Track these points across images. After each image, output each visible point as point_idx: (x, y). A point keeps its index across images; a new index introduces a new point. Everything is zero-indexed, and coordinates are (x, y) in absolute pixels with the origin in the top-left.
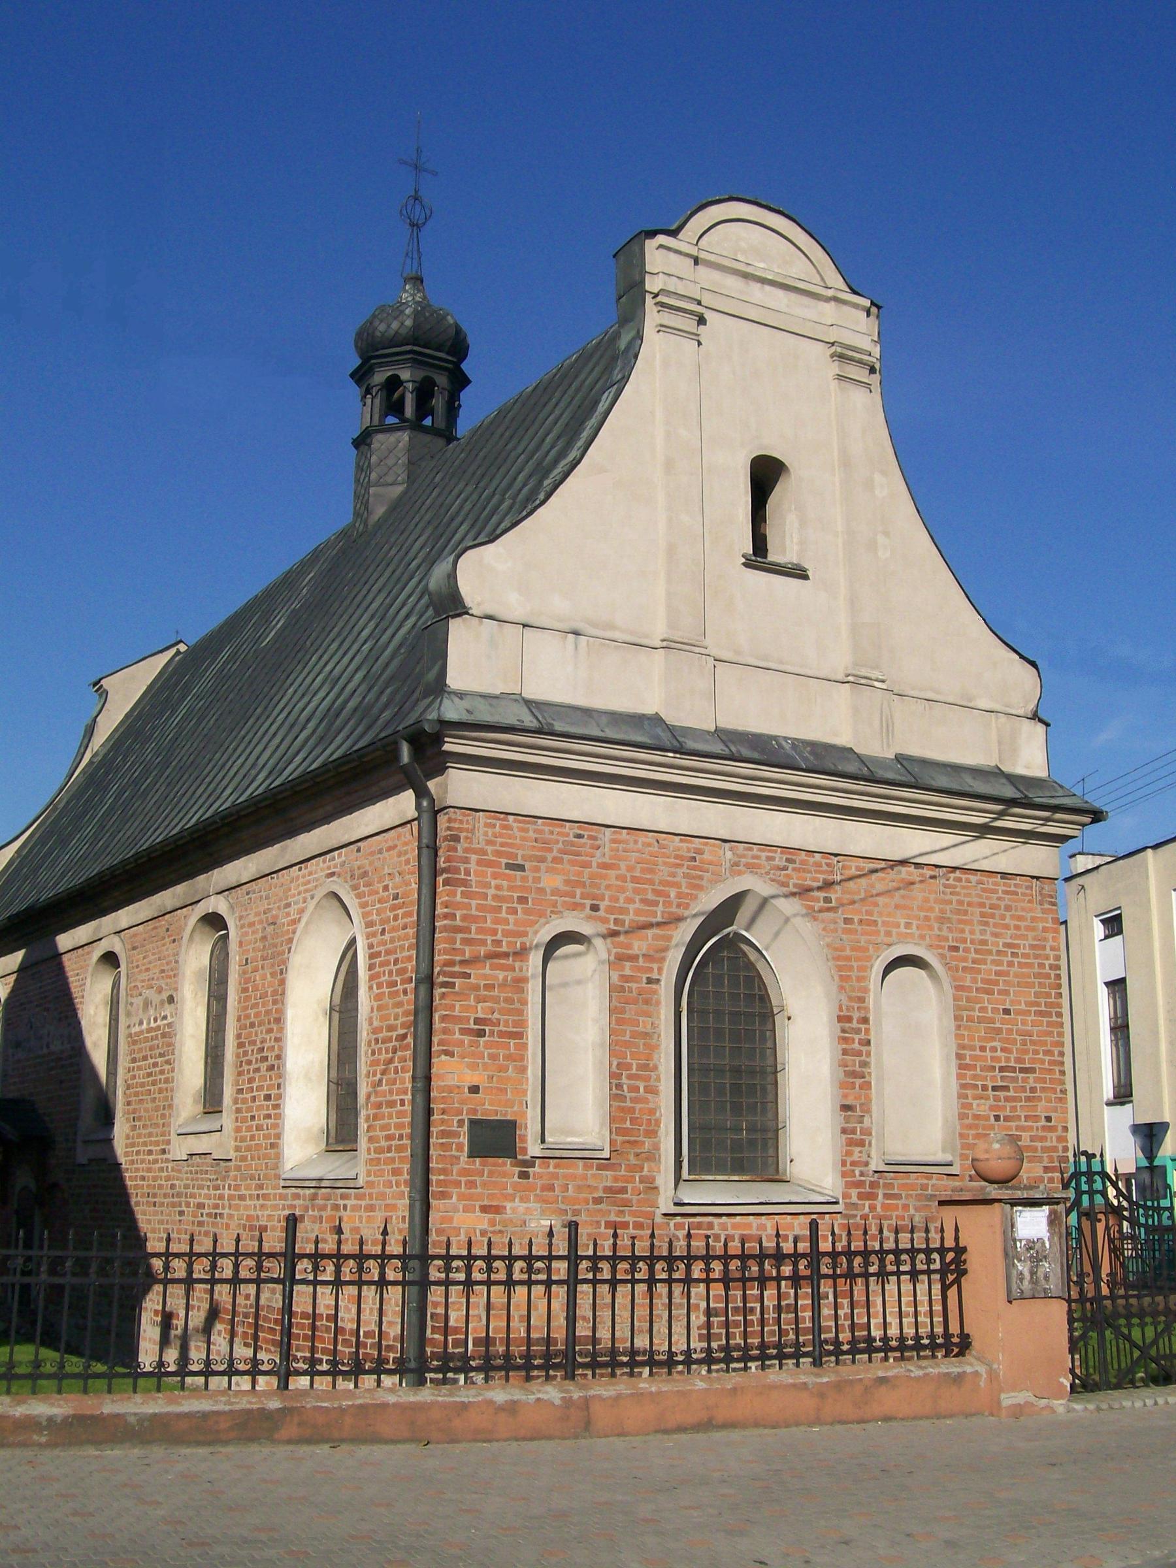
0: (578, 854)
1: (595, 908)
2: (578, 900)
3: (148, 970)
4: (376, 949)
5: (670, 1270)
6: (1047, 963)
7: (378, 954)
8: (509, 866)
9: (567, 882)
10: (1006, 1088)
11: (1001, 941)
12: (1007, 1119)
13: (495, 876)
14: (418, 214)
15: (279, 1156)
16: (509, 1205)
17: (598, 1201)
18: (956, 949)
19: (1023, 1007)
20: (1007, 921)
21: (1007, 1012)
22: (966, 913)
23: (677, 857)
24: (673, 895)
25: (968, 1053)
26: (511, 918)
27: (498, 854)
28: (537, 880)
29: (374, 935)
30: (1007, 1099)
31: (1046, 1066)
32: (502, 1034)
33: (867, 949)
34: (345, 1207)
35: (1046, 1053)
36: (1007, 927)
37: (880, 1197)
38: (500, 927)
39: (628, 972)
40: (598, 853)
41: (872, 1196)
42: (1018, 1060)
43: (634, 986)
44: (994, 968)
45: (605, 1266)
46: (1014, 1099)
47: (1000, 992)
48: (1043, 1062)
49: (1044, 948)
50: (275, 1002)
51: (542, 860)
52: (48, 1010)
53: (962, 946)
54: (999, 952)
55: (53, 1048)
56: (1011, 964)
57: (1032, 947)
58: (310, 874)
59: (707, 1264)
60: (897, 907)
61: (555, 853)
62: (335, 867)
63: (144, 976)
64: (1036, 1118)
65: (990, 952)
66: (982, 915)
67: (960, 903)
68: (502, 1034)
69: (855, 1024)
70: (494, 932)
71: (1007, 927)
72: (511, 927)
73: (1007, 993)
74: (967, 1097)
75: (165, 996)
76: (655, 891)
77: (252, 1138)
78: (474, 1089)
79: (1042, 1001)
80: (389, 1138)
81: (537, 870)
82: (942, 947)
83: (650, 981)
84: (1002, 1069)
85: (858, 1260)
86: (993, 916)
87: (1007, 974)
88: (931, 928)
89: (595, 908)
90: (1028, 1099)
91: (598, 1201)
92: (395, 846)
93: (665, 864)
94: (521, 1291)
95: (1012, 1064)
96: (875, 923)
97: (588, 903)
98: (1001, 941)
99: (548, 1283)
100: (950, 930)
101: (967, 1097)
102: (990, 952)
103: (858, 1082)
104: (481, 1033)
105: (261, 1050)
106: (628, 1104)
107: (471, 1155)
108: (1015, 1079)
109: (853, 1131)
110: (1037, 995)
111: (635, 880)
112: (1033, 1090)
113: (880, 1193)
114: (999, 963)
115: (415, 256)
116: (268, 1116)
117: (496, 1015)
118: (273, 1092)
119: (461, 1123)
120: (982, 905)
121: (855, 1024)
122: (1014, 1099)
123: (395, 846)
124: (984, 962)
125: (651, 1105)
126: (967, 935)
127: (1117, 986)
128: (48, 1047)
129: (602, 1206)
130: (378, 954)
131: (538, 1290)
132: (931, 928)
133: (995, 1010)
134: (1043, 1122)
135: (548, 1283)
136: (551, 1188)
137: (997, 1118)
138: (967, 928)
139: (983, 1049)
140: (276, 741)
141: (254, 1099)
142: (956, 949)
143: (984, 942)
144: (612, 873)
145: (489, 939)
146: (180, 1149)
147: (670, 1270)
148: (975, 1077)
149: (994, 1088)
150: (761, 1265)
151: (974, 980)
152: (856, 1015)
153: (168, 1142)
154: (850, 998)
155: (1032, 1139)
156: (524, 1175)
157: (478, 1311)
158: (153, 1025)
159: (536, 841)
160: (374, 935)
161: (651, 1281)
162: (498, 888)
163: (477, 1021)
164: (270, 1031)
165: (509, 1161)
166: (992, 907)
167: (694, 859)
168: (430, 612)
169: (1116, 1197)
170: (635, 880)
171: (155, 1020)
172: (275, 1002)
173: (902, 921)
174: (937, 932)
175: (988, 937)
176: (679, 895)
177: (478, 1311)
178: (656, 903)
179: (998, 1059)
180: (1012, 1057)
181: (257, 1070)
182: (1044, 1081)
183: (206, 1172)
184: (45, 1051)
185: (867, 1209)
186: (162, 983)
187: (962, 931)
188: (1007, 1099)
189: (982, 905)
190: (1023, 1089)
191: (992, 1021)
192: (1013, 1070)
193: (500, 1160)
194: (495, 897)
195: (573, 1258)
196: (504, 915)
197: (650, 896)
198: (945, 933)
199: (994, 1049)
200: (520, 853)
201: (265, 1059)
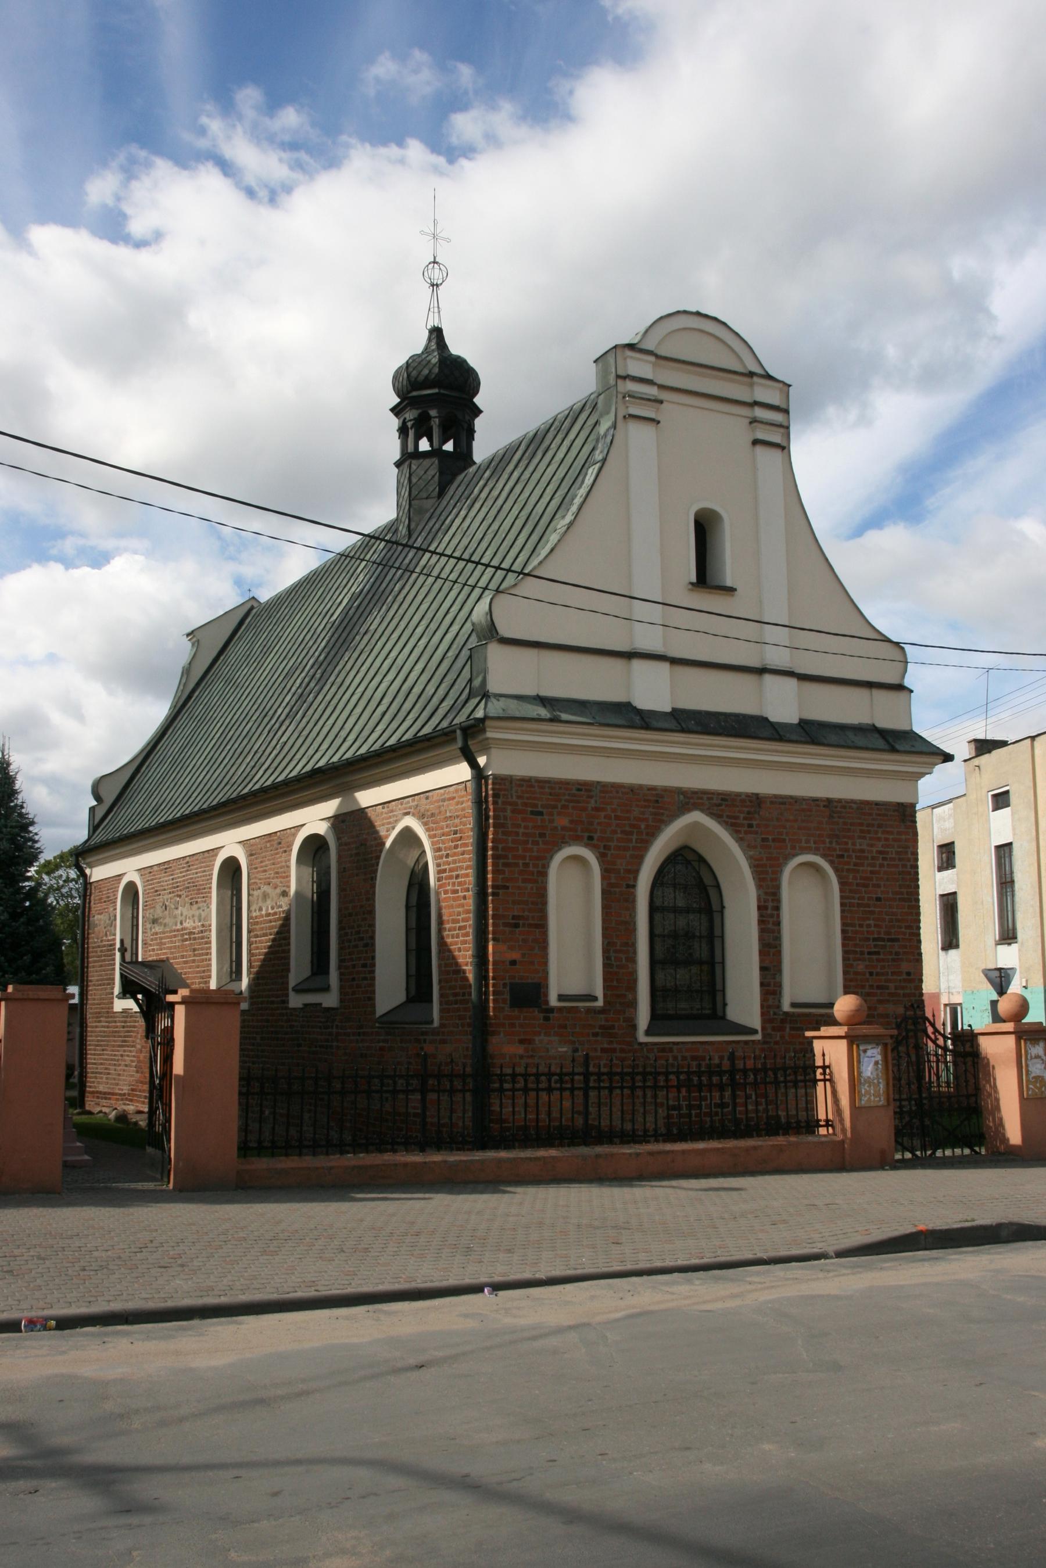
0: (578, 802)
1: (591, 838)
2: (579, 833)
3: (265, 871)
4: (443, 867)
5: (644, 1081)
6: (909, 864)
7: (444, 871)
8: (532, 813)
9: (571, 822)
10: (878, 953)
11: (874, 849)
12: (878, 974)
13: (524, 820)
14: (437, 275)
15: (373, 1006)
16: (537, 1038)
17: (595, 1035)
18: (842, 856)
19: (890, 895)
20: (879, 835)
21: (878, 899)
22: (849, 830)
23: (645, 801)
24: (643, 827)
25: (850, 929)
26: (535, 848)
27: (525, 805)
28: (551, 821)
29: (441, 857)
30: (878, 960)
31: (907, 936)
32: (530, 925)
33: (778, 859)
34: (425, 1041)
35: (907, 927)
36: (879, 839)
37: (788, 1029)
38: (528, 854)
39: (613, 881)
40: (593, 801)
41: (781, 1029)
42: (888, 933)
43: (617, 890)
44: (869, 869)
45: (521, 1079)
46: (883, 960)
47: (874, 886)
48: (904, 934)
49: (907, 853)
50: (368, 899)
51: (555, 807)
52: (180, 896)
53: (846, 854)
54: (873, 858)
55: (185, 925)
56: (882, 866)
57: (897, 853)
58: (392, 811)
59: (667, 1077)
60: (799, 828)
61: (563, 802)
62: (410, 808)
63: (261, 875)
64: (900, 973)
65: (867, 858)
66: (862, 831)
67: (845, 823)
68: (530, 925)
69: (769, 911)
70: (524, 858)
71: (879, 839)
72: (535, 854)
73: (879, 886)
74: (849, 959)
75: (278, 891)
76: (631, 826)
77: (354, 993)
78: (513, 963)
79: (904, 890)
80: (455, 995)
81: (551, 814)
82: (832, 856)
83: (628, 886)
84: (875, 940)
85: (662, 1078)
86: (869, 832)
87: (878, 872)
88: (824, 842)
89: (591, 838)
90: (893, 960)
91: (595, 1035)
92: (454, 798)
93: (637, 806)
94: (557, 1093)
95: (882, 936)
96: (784, 841)
97: (586, 834)
98: (874, 849)
99: (572, 1090)
100: (838, 843)
101: (849, 959)
102: (867, 858)
103: (772, 950)
104: (516, 926)
105: (358, 932)
106: (615, 969)
107: (512, 1006)
108: (884, 947)
109: (769, 985)
110: (900, 886)
111: (617, 818)
112: (897, 954)
113: (788, 1026)
114: (874, 865)
115: (436, 310)
116: (365, 979)
117: (526, 913)
118: (369, 962)
119: (505, 985)
120: (861, 824)
121: (769, 911)
122: (883, 960)
123: (454, 798)
124: (862, 865)
125: (631, 970)
126: (850, 846)
127: (1004, 851)
128: (181, 923)
129: (599, 1038)
130: (444, 871)
131: (567, 1093)
132: (824, 842)
133: (870, 899)
134: (904, 976)
135: (572, 1090)
136: (565, 1027)
137: (871, 974)
138: (850, 842)
139: (861, 926)
140: (358, 710)
141: (354, 966)
142: (842, 856)
143: (862, 851)
144: (603, 814)
145: (521, 862)
146: (296, 1001)
147: (644, 1081)
148: (855, 945)
149: (869, 953)
150: (451, 1082)
151: (855, 878)
152: (770, 904)
153: (287, 995)
154: (766, 893)
155: (896, 988)
156: (547, 1019)
157: (519, 1109)
158: (270, 911)
159: (551, 794)
160: (441, 857)
161: (633, 1088)
162: (526, 827)
163: (514, 917)
164: (365, 919)
165: (536, 1010)
166: (868, 825)
167: (657, 801)
168: (474, 637)
169: (934, 1033)
170: (617, 818)
171: (273, 908)
172: (368, 899)
173: (804, 838)
174: (828, 845)
175: (864, 847)
176: (647, 827)
177: (519, 1109)
178: (632, 833)
179: (872, 933)
180: (882, 930)
181: (356, 946)
182: (905, 947)
183: (318, 1017)
184: (179, 927)
185: (778, 1039)
186: (277, 881)
187: (846, 843)
188: (878, 960)
189: (861, 824)
190: (891, 953)
191: (868, 906)
192: (883, 940)
193: (531, 1010)
194: (524, 834)
195: (586, 1075)
196: (530, 846)
197: (627, 829)
198: (834, 845)
199: (869, 926)
200: (540, 803)
201: (362, 939)
